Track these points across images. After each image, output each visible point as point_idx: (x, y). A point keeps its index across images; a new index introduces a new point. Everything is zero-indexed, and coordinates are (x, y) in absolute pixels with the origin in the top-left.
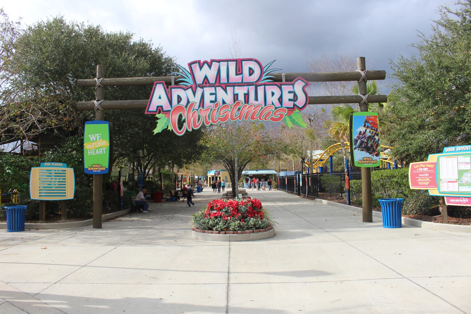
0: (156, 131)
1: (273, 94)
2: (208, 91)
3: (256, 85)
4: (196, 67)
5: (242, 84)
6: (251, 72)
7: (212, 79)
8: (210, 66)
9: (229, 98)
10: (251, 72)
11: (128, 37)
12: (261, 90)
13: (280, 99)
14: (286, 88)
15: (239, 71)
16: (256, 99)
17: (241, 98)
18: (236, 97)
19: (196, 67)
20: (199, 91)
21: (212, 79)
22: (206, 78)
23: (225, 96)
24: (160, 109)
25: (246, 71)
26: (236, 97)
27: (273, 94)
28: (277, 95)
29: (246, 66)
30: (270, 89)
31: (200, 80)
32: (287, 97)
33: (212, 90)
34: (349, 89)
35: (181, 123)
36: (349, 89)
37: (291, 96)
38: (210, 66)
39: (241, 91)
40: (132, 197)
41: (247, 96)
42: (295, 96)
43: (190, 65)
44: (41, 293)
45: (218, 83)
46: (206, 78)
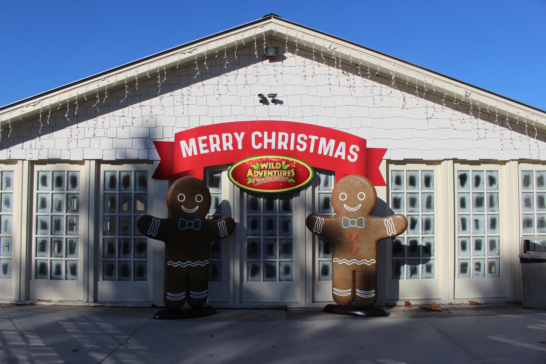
0: (294, 182)
2: (265, 171)
3: (279, 170)
5: (275, 169)
7: (266, 168)
9: (271, 173)
10: (278, 166)
12: (281, 171)
15: (275, 166)
17: (275, 174)
18: (273, 173)
20: (262, 171)
21: (266, 168)
23: (270, 173)
24: (250, 176)
25: (277, 165)
26: (273, 173)
29: (277, 164)
32: (289, 173)
33: (266, 171)
35: (256, 183)
39: (275, 172)
40: (332, 178)
41: (277, 173)
42: (292, 174)
44: (318, 187)
45: (268, 169)
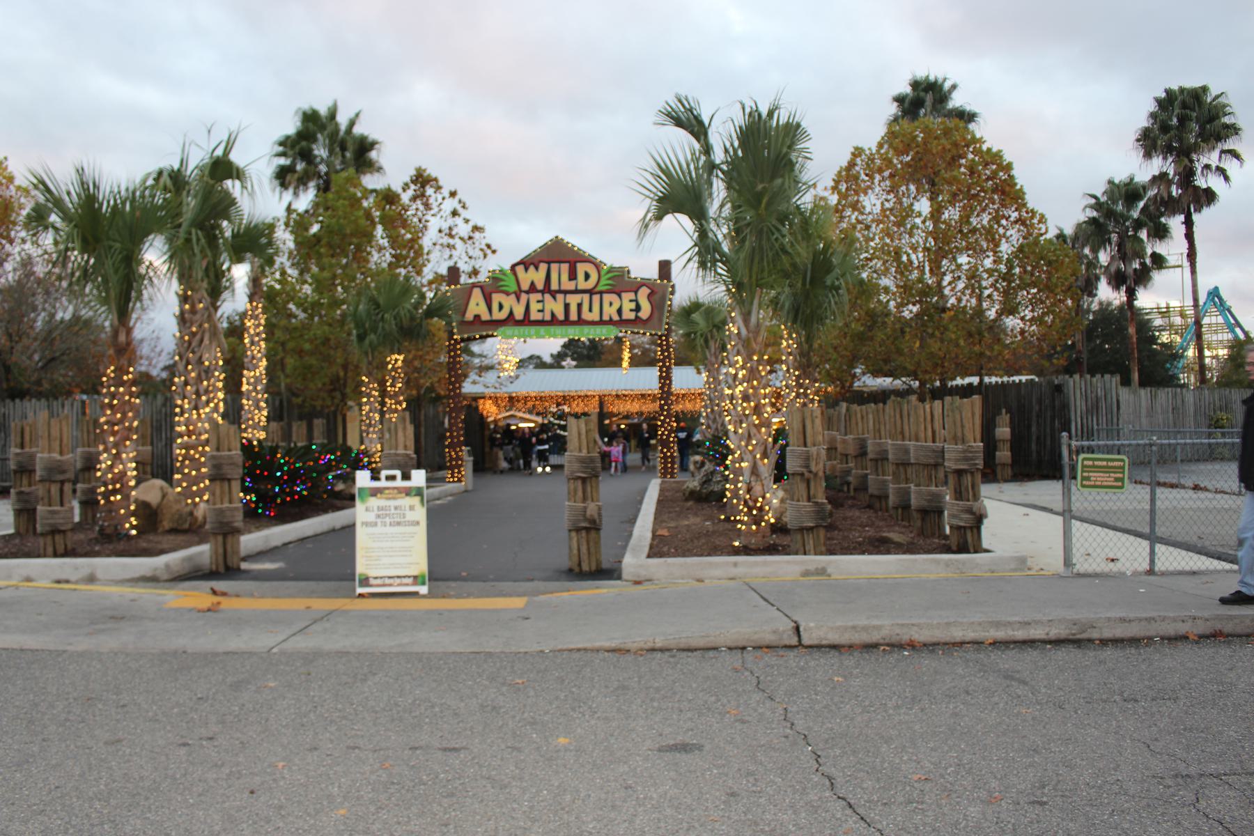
1: (611, 304)
2: (534, 297)
3: (591, 292)
4: (520, 269)
5: (576, 291)
6: (587, 276)
7: (540, 286)
8: (537, 268)
10: (587, 276)
11: (1205, 89)
13: (619, 311)
14: (628, 296)
16: (590, 310)
19: (520, 269)
21: (540, 286)
22: (532, 284)
25: (581, 276)
27: (611, 304)
28: (616, 306)
30: (607, 298)
31: (525, 286)
33: (539, 296)
34: (959, 434)
36: (959, 434)
37: (633, 305)
38: (537, 268)
39: (573, 300)
43: (513, 267)
45: (547, 289)
46: (532, 284)
